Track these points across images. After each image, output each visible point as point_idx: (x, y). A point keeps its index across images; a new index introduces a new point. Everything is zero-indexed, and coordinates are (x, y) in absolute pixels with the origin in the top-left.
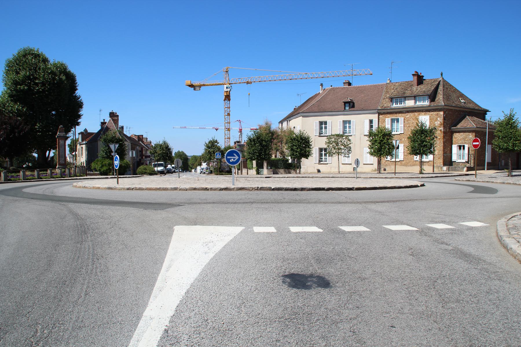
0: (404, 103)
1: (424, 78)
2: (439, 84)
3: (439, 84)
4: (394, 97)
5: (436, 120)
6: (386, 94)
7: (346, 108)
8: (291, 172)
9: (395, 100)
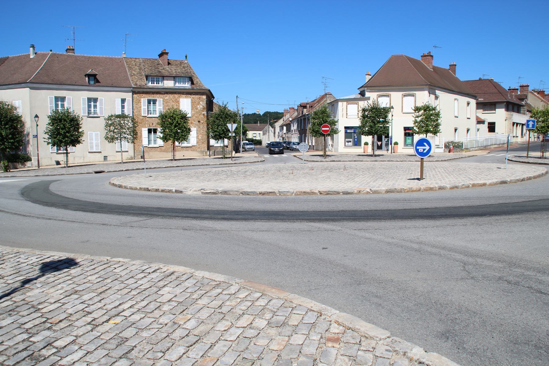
5: (199, 104)
7: (90, 82)
8: (18, 167)
9: (150, 78)
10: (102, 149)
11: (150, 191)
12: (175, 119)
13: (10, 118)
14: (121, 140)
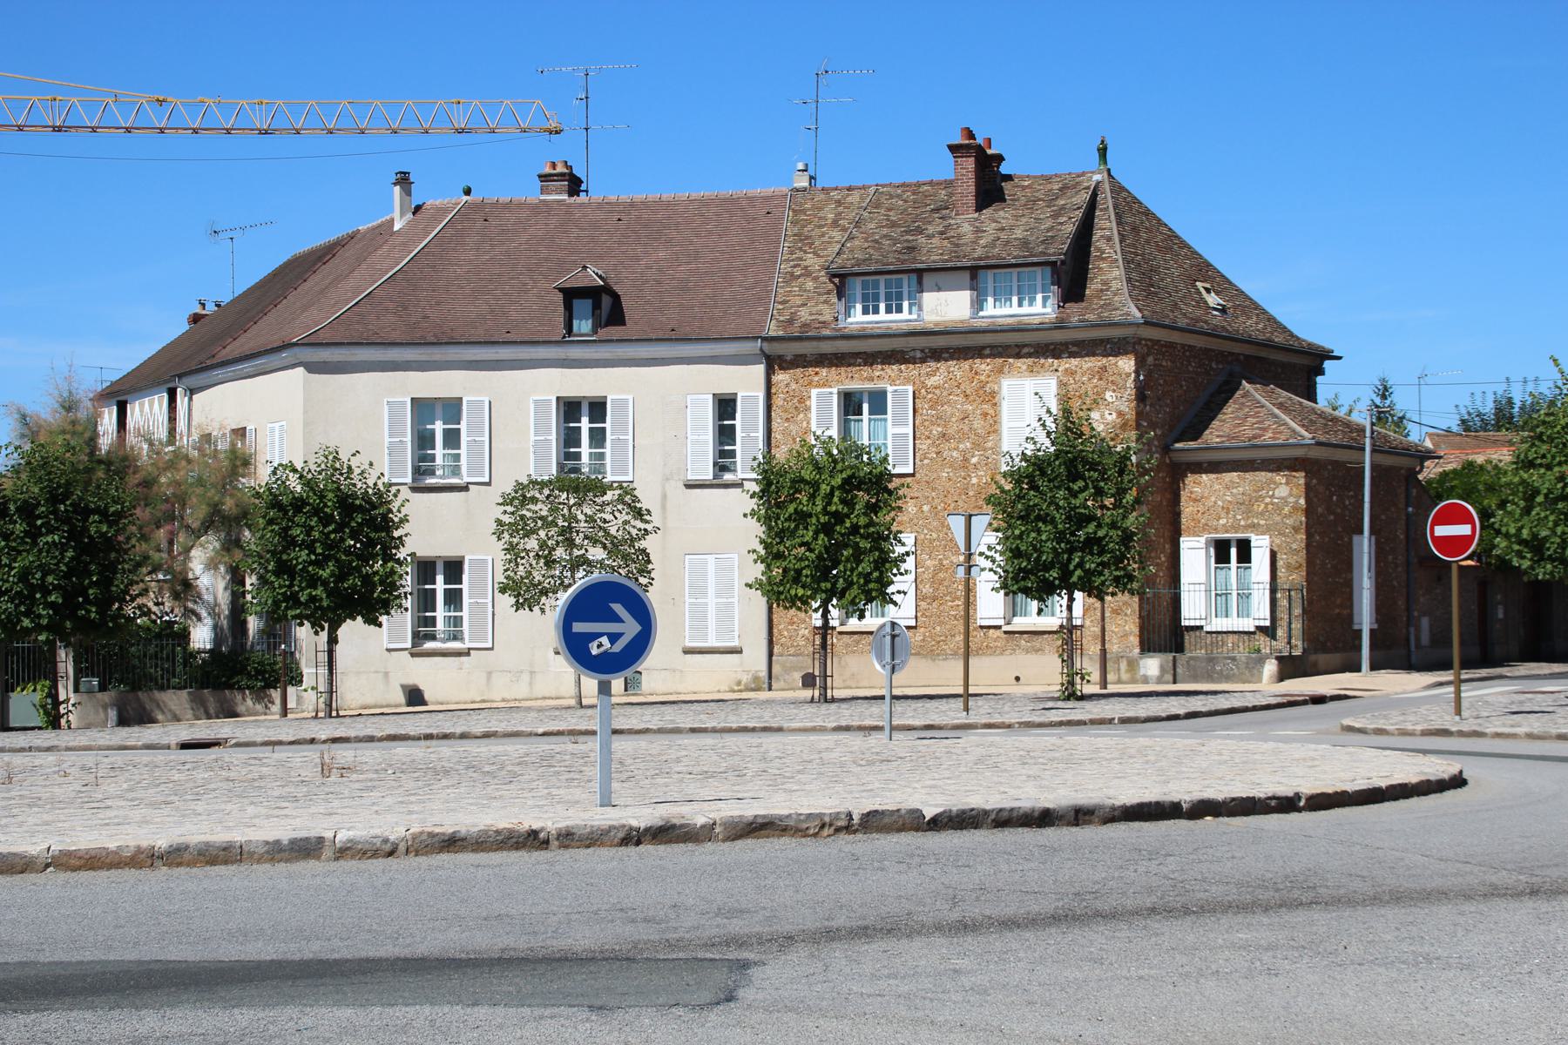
0: (910, 306)
1: (1004, 169)
2: (1092, 205)
3: (1092, 205)
4: (856, 269)
6: (799, 254)
7: (575, 323)
8: (241, 708)
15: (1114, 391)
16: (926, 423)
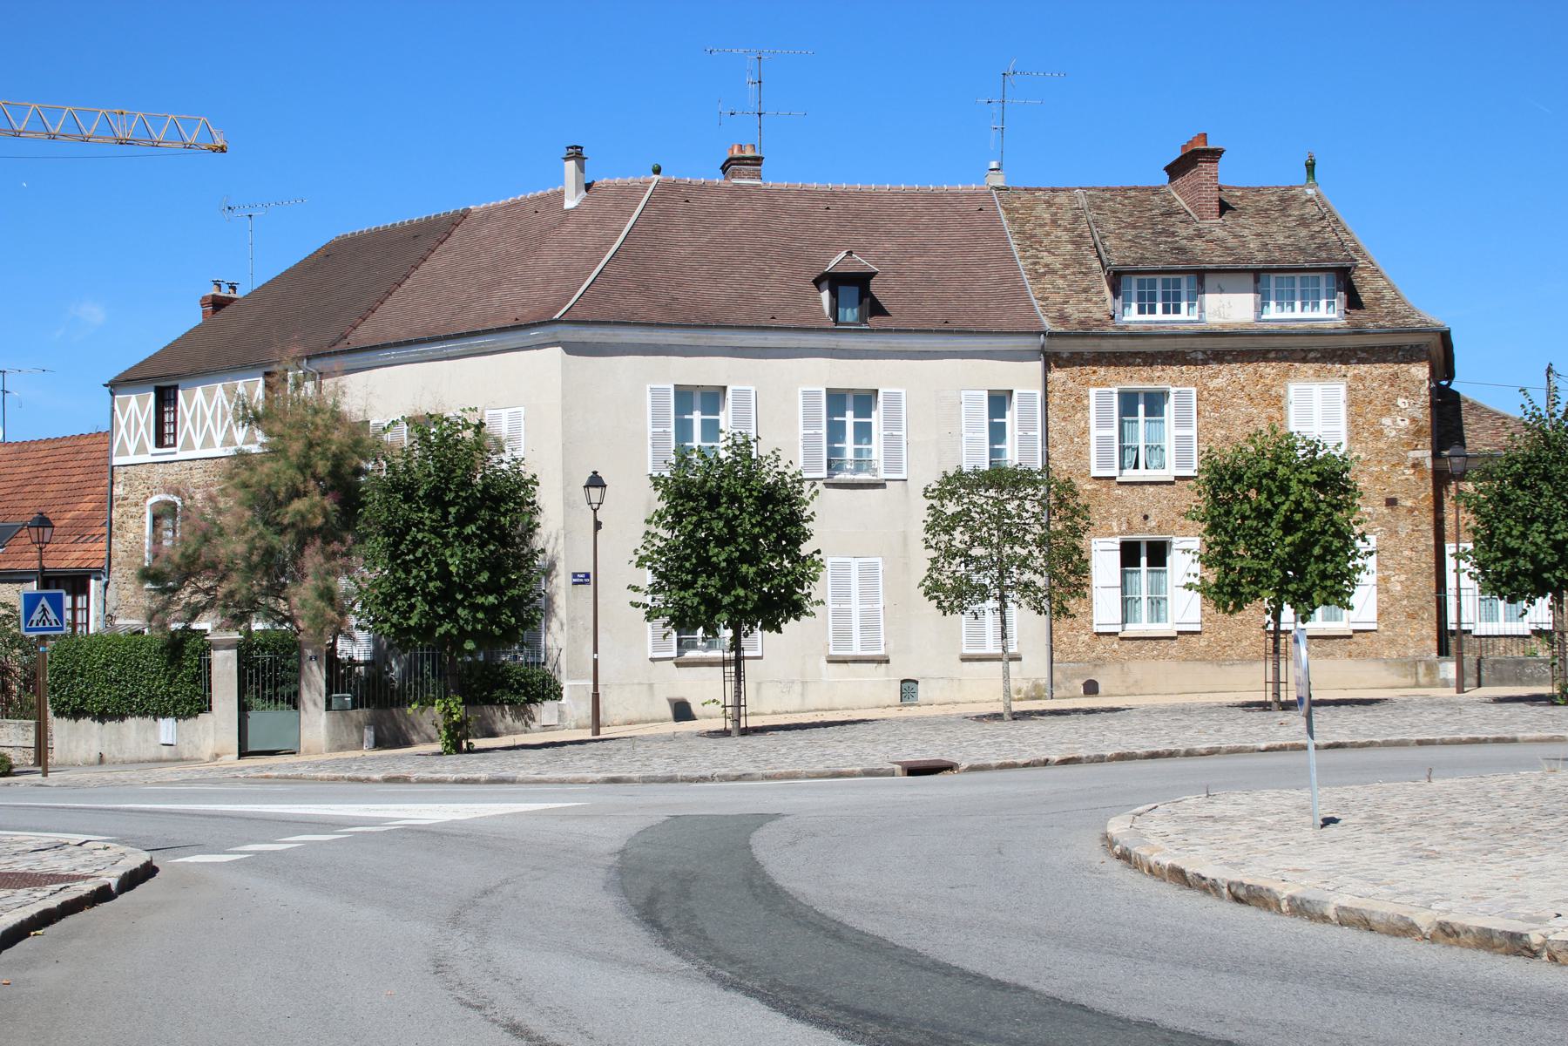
5: (1389, 406)
8: (500, 727)
10: (891, 645)
11: (1535, 954)
12: (1284, 490)
13: (486, 487)
14: (1002, 598)
15: (1407, 398)
16: (1209, 426)
